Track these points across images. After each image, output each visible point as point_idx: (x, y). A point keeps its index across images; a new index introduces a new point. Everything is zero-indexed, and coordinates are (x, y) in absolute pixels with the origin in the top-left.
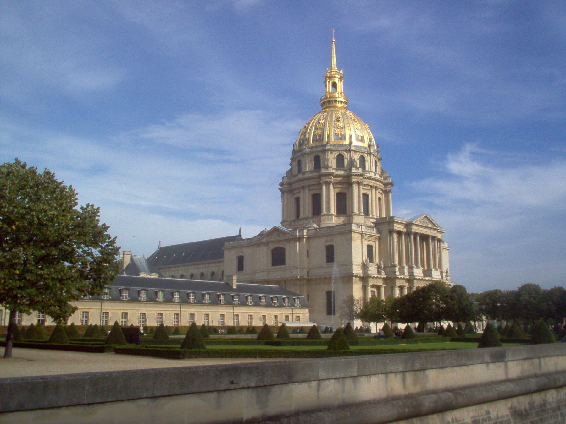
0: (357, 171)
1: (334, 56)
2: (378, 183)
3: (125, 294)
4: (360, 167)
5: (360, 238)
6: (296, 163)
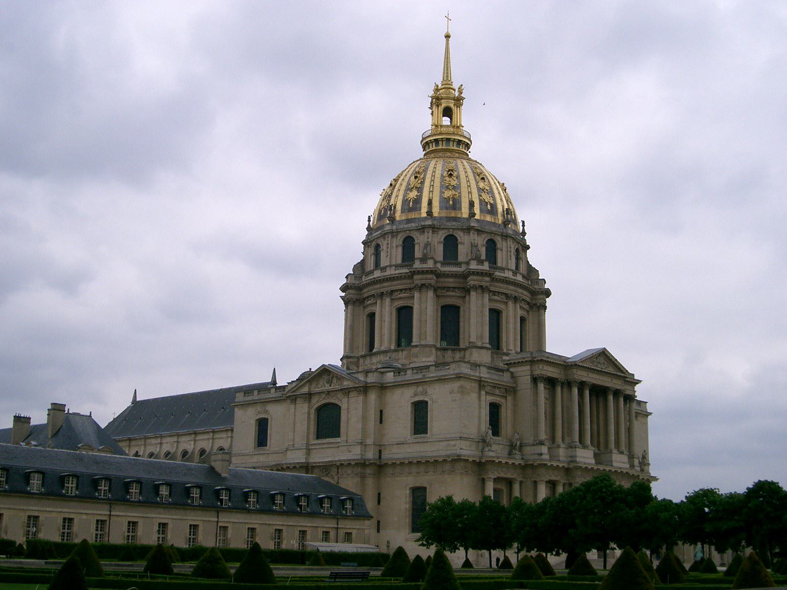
0: (480, 267)
2: (520, 290)
3: (35, 482)
4: (486, 260)
5: (477, 390)
6: (371, 250)
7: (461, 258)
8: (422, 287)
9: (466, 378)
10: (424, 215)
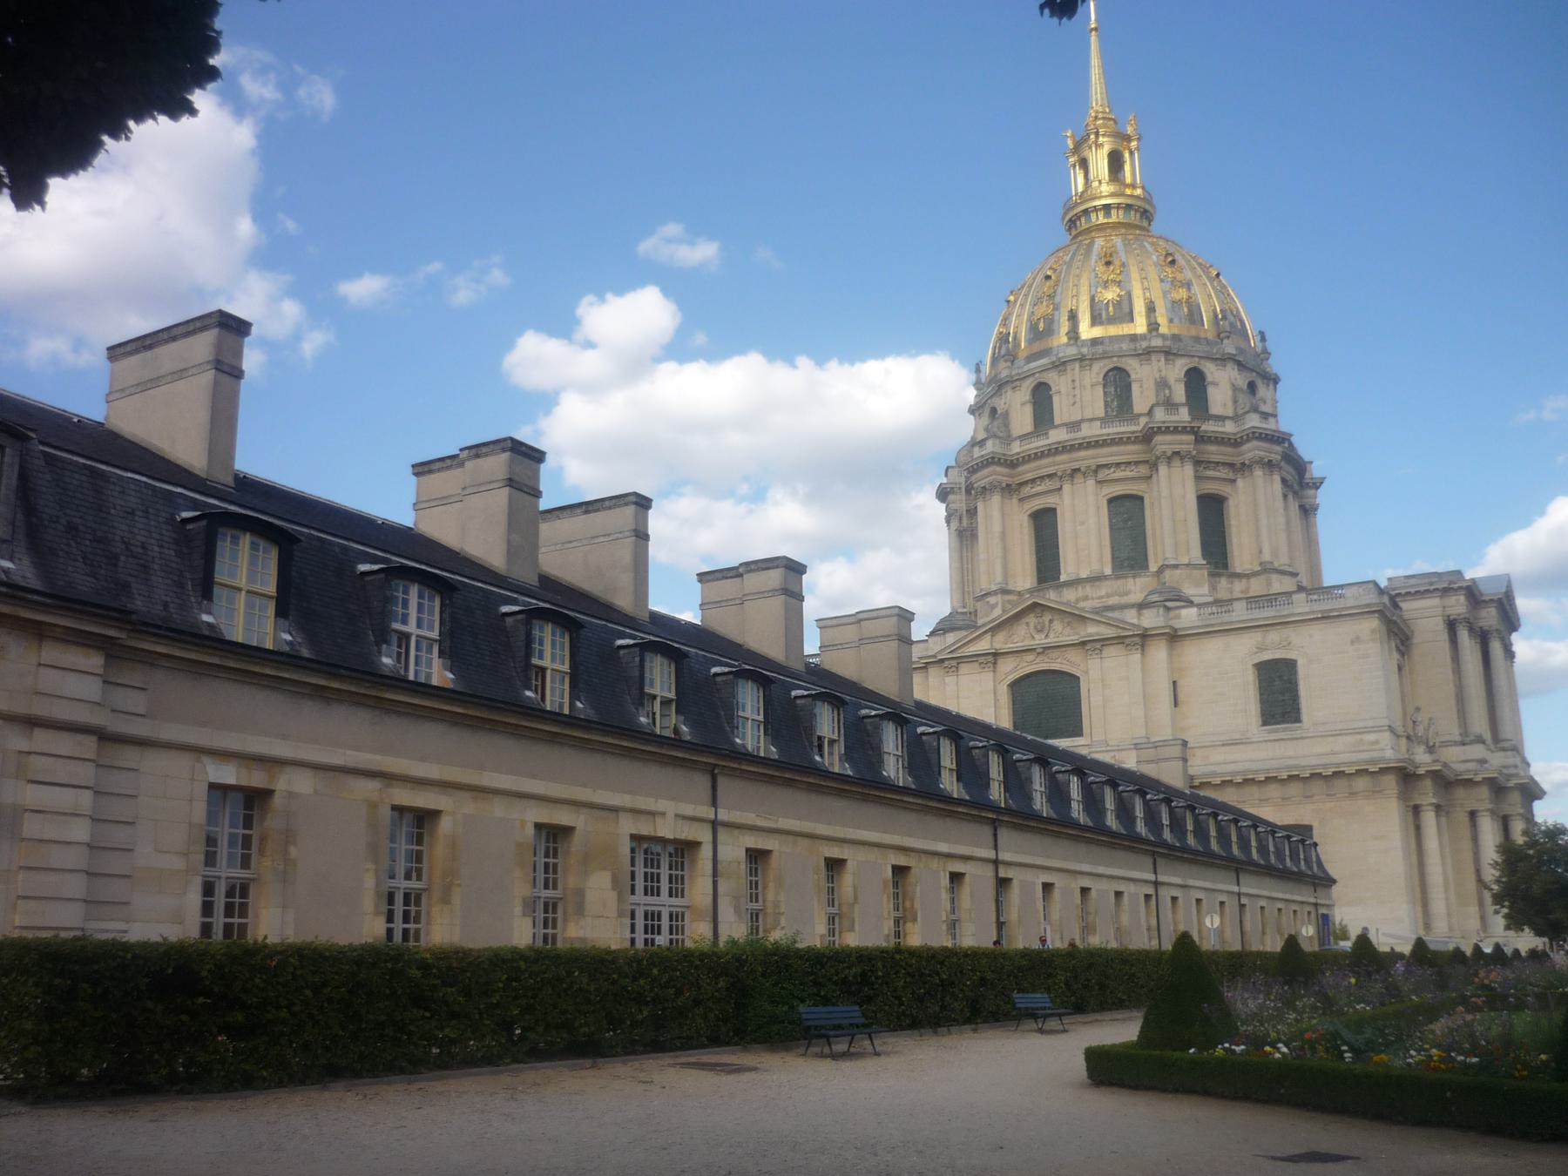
1: (1095, 61)
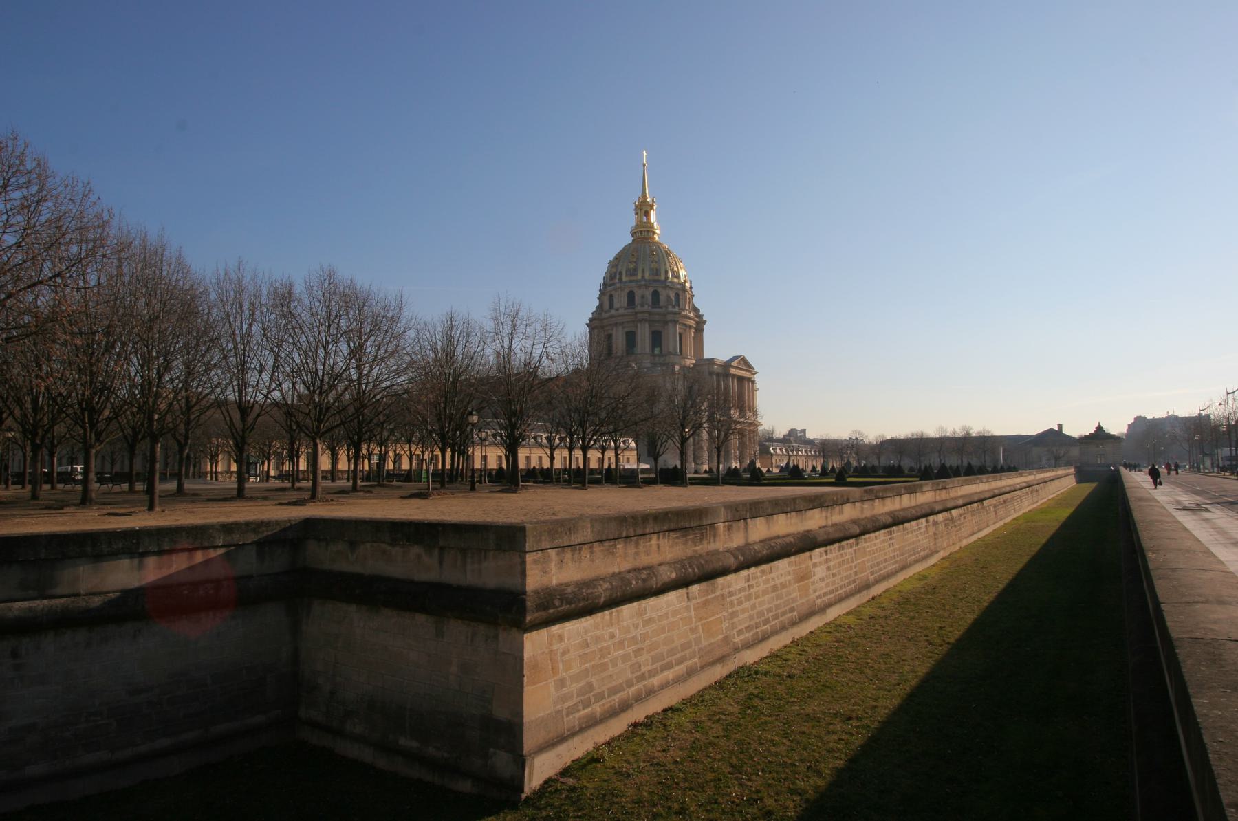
7: (662, 303)
8: (641, 321)
9: (225, 500)
10: (639, 277)
